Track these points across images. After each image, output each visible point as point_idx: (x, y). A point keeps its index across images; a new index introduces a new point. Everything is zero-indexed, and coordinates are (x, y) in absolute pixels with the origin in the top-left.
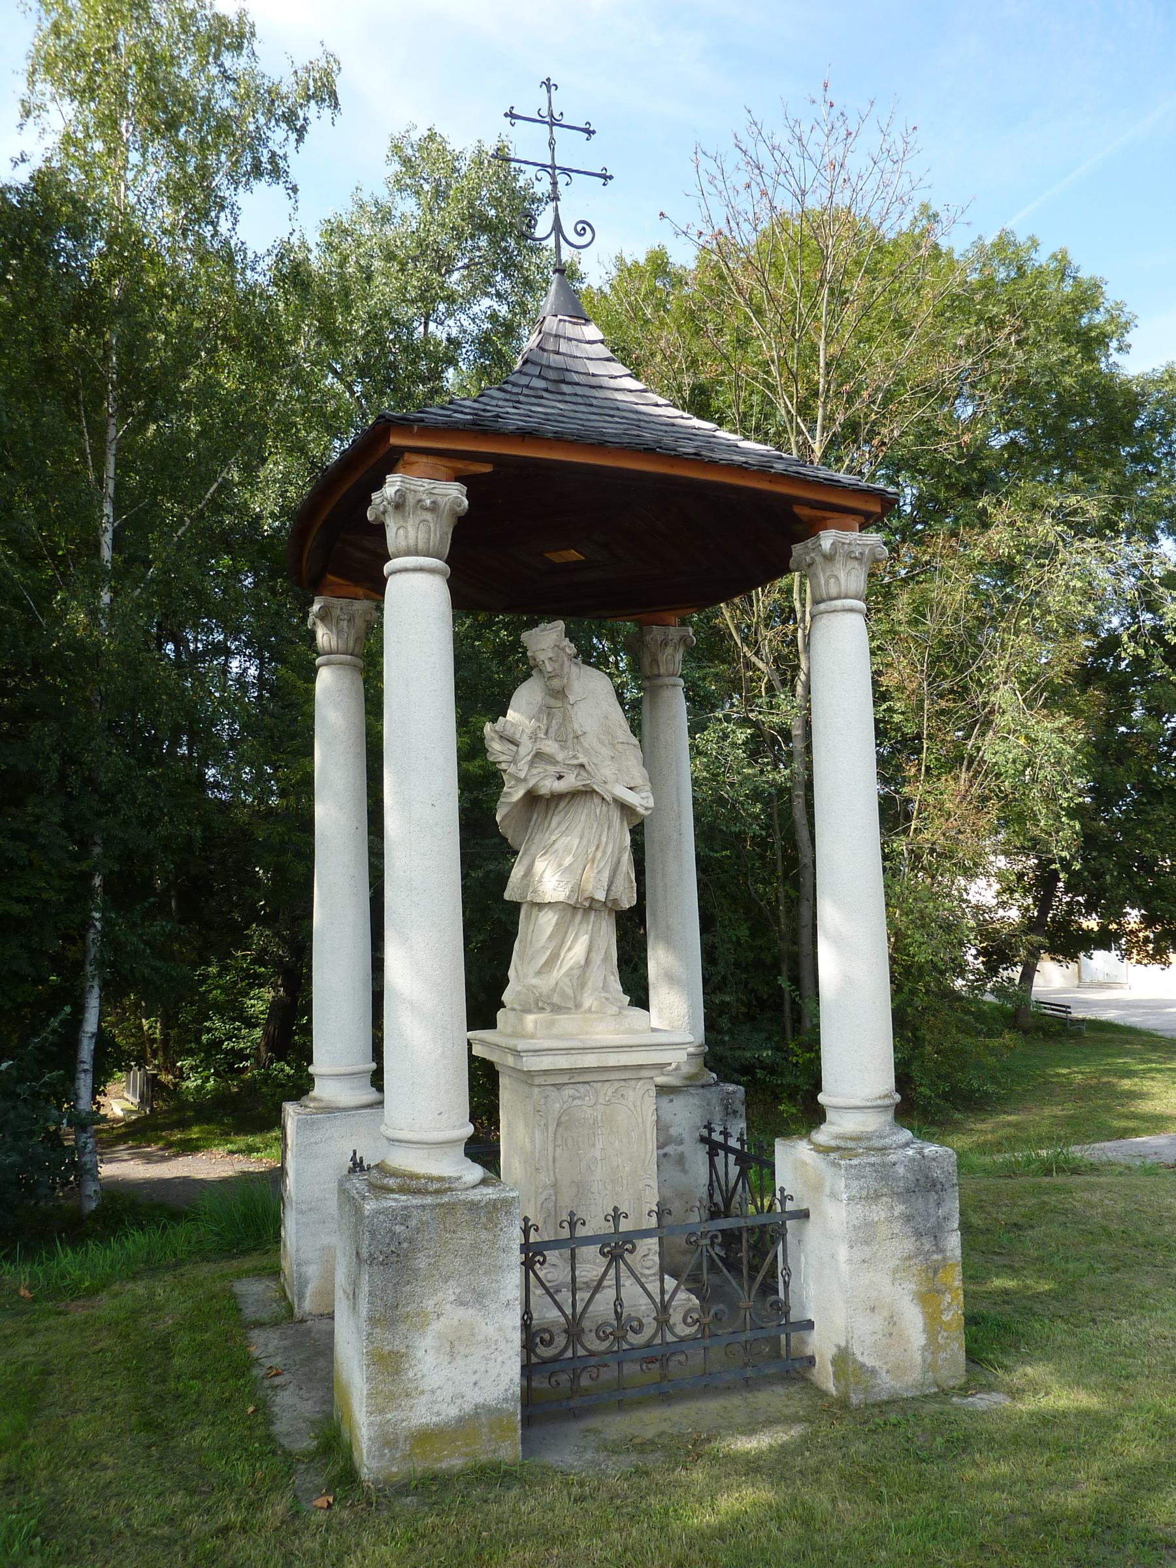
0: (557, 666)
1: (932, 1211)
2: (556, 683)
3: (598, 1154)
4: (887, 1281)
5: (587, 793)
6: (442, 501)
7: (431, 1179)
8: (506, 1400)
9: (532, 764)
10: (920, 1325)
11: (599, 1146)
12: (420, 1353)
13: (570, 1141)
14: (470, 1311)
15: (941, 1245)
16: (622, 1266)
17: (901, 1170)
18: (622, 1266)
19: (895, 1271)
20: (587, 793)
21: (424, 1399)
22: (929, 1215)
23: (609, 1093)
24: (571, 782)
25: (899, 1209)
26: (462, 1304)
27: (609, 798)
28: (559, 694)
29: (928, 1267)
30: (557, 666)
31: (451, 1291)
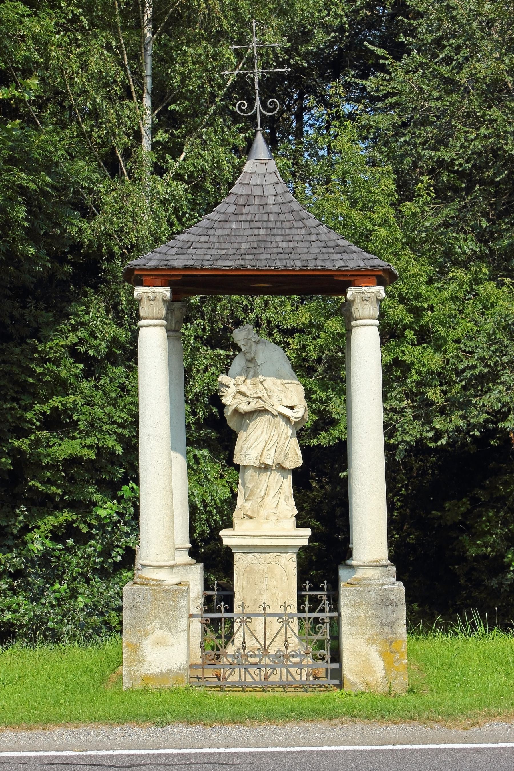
0: (247, 348)
1: (390, 615)
2: (249, 356)
3: (265, 587)
4: (364, 644)
5: (262, 412)
6: (157, 295)
7: (152, 580)
8: (180, 669)
9: (234, 397)
10: (382, 667)
11: (266, 583)
12: (145, 646)
13: (251, 580)
14: (165, 632)
15: (394, 631)
16: (245, 627)
17: (373, 594)
18: (245, 627)
19: (368, 640)
20: (262, 412)
21: (146, 664)
22: (388, 616)
23: (271, 557)
24: (254, 406)
25: (371, 612)
26: (161, 629)
27: (275, 413)
28: (252, 360)
29: (387, 640)
30: (247, 348)
31: (156, 624)
